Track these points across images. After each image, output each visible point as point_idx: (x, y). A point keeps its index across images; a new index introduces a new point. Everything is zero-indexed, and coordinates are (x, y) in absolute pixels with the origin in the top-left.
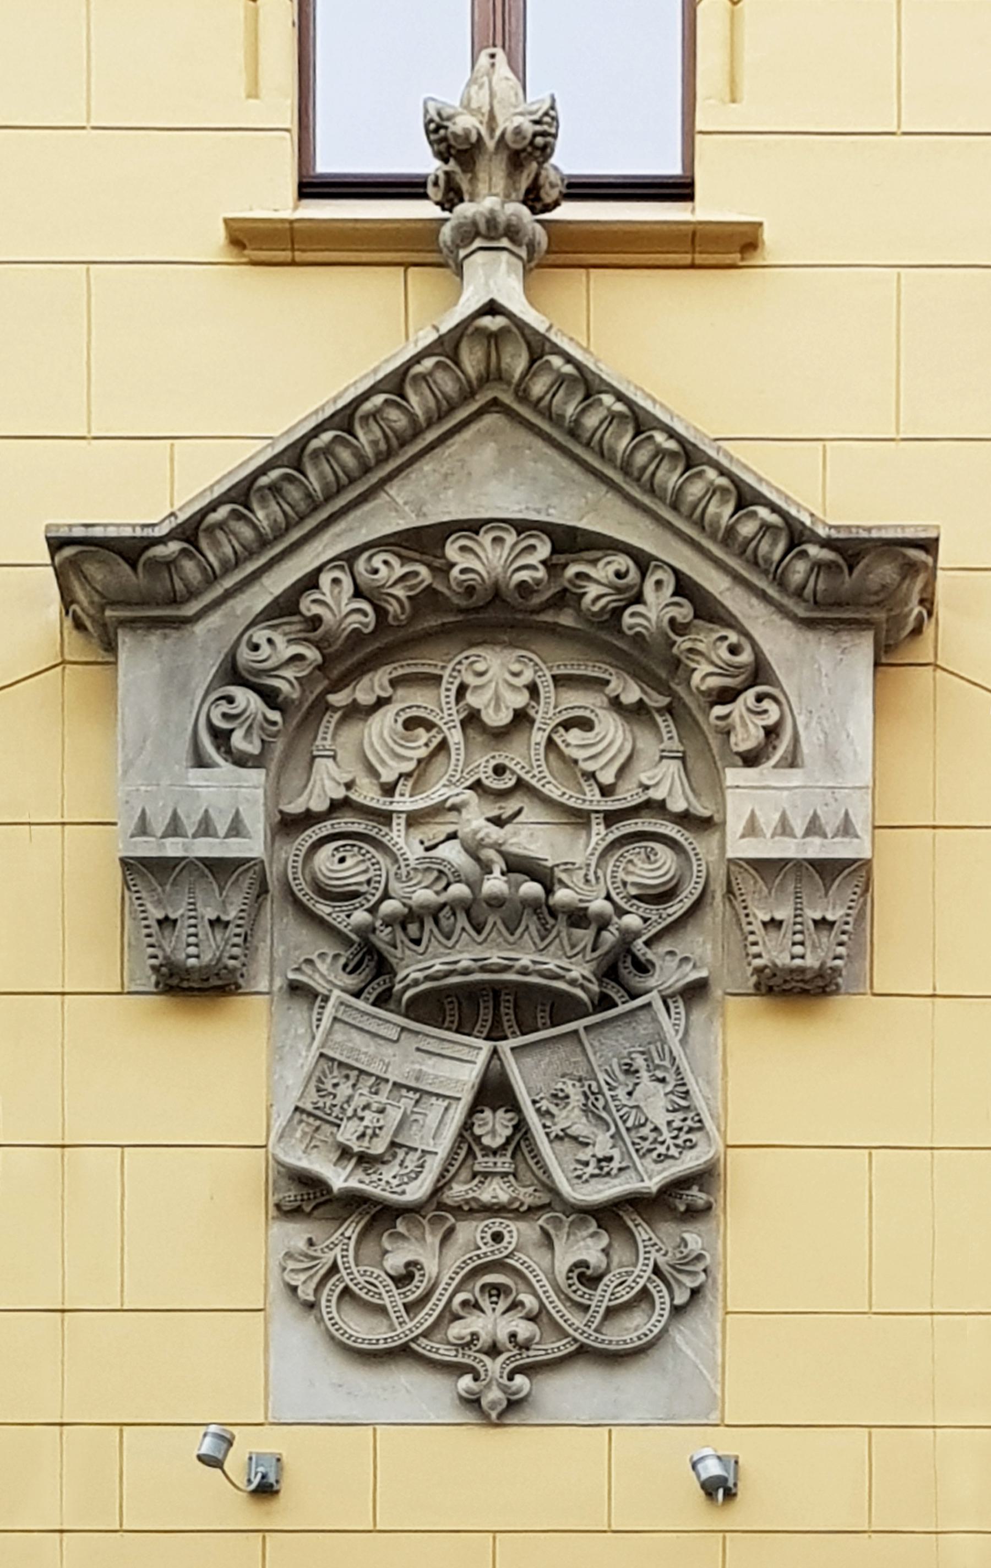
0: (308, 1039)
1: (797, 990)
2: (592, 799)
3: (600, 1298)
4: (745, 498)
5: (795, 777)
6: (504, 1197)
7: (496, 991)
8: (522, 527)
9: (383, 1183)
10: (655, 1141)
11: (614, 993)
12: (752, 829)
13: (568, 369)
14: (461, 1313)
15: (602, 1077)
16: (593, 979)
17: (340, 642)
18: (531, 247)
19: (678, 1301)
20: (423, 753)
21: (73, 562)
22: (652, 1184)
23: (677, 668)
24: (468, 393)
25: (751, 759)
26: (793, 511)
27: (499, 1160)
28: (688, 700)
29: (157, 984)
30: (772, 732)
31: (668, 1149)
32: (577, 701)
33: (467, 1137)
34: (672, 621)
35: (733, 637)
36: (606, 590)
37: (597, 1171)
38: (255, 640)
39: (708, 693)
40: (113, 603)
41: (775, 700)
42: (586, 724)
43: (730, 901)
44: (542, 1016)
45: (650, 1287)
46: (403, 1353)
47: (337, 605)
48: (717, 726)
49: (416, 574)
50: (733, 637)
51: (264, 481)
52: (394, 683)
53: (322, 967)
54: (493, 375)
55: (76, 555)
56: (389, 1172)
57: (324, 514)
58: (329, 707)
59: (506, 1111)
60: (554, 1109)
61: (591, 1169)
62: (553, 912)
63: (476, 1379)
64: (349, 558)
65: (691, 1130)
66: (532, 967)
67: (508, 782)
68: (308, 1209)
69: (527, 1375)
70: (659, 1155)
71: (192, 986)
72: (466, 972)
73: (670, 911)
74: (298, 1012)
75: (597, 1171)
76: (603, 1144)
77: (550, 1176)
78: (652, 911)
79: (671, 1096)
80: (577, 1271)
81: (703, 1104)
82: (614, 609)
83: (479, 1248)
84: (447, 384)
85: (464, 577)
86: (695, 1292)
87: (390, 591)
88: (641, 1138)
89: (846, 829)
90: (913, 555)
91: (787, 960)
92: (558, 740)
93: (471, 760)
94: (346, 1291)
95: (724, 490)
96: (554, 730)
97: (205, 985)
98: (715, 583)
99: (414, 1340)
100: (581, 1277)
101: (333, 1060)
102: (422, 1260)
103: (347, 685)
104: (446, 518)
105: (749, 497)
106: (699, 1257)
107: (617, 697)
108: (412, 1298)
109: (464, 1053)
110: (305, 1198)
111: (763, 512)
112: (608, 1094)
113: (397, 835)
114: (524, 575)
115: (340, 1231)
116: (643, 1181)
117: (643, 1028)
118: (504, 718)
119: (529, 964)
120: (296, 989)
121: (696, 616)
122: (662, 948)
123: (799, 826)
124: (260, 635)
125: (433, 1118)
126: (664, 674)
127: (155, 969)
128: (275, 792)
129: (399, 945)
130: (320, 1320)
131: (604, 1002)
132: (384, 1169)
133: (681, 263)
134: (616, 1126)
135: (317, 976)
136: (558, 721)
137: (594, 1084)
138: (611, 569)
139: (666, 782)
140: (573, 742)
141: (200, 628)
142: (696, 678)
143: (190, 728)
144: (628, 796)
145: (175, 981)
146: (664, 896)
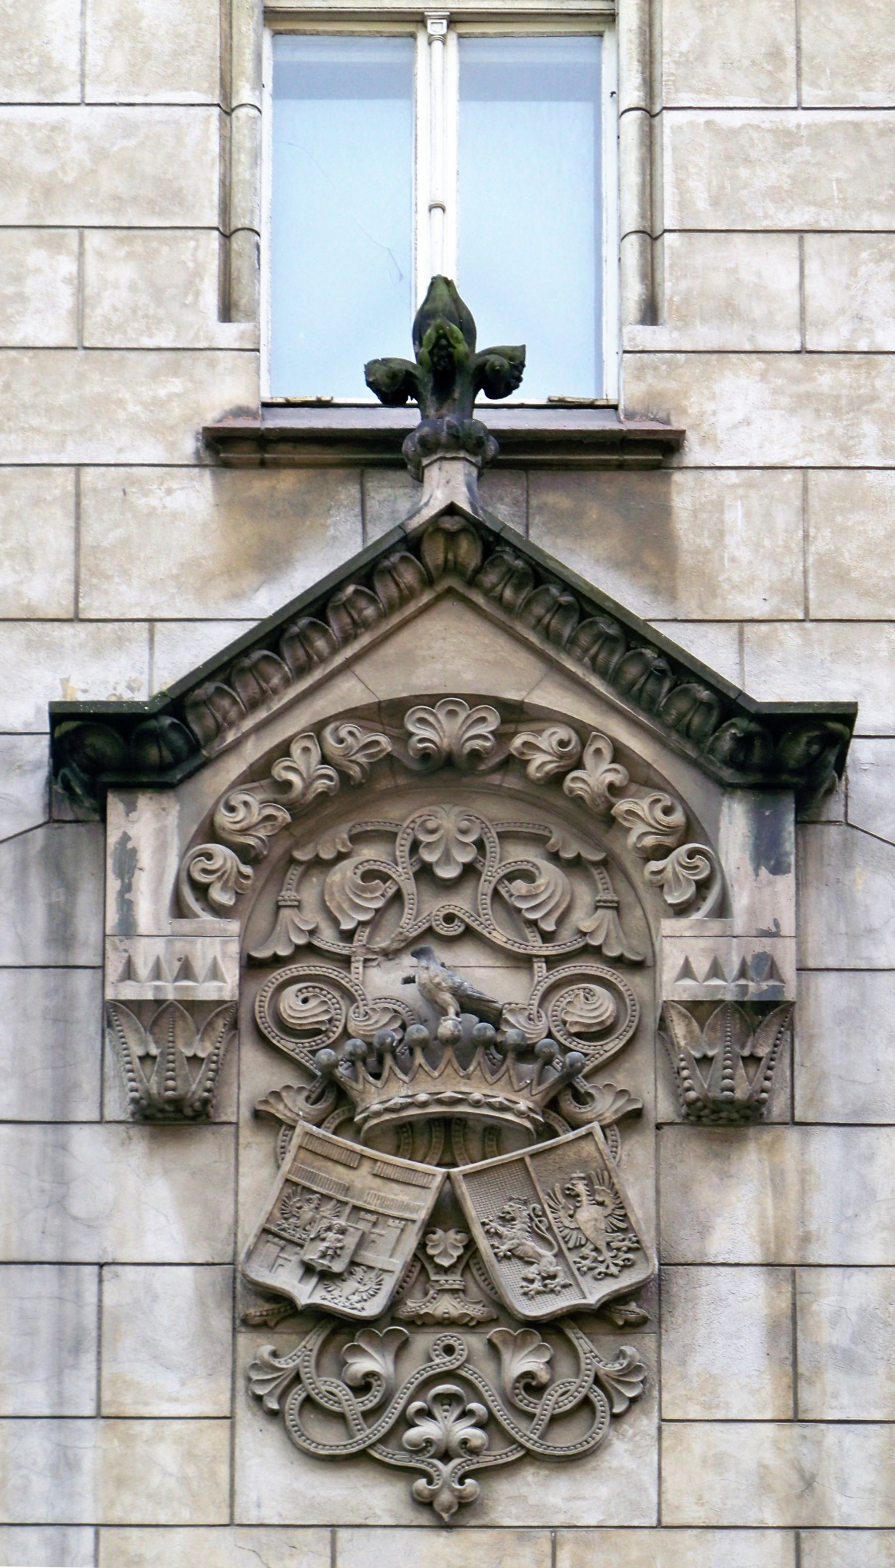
1: (726, 1119)
2: (536, 946)
8: (475, 700)
10: (595, 1260)
12: (687, 971)
19: (616, 1410)
25: (682, 910)
27: (450, 1278)
31: (608, 1267)
32: (522, 855)
33: (421, 1259)
35: (667, 801)
36: (549, 758)
38: (233, 803)
39: (643, 849)
41: (708, 859)
42: (528, 876)
44: (475, 1147)
45: (592, 1396)
47: (303, 771)
48: (651, 881)
49: (377, 743)
50: (667, 801)
58: (293, 861)
62: (500, 1047)
63: (430, 1482)
64: (318, 728)
65: (630, 1250)
66: (484, 1099)
67: (456, 929)
68: (272, 1324)
69: (477, 1479)
71: (170, 1118)
72: (424, 1104)
73: (606, 1048)
75: (541, 1288)
76: (548, 1259)
79: (610, 1219)
80: (523, 1382)
85: (421, 746)
86: (633, 1401)
87: (353, 758)
90: (831, 727)
92: (503, 891)
94: (309, 1401)
96: (500, 881)
99: (372, 1446)
107: (557, 852)
108: (370, 1406)
114: (477, 744)
115: (303, 1343)
116: (585, 1298)
119: (482, 1098)
122: (601, 1081)
124: (237, 799)
127: (134, 1101)
131: (548, 1132)
136: (502, 874)
138: (554, 740)
144: (567, 941)
146: (603, 1032)
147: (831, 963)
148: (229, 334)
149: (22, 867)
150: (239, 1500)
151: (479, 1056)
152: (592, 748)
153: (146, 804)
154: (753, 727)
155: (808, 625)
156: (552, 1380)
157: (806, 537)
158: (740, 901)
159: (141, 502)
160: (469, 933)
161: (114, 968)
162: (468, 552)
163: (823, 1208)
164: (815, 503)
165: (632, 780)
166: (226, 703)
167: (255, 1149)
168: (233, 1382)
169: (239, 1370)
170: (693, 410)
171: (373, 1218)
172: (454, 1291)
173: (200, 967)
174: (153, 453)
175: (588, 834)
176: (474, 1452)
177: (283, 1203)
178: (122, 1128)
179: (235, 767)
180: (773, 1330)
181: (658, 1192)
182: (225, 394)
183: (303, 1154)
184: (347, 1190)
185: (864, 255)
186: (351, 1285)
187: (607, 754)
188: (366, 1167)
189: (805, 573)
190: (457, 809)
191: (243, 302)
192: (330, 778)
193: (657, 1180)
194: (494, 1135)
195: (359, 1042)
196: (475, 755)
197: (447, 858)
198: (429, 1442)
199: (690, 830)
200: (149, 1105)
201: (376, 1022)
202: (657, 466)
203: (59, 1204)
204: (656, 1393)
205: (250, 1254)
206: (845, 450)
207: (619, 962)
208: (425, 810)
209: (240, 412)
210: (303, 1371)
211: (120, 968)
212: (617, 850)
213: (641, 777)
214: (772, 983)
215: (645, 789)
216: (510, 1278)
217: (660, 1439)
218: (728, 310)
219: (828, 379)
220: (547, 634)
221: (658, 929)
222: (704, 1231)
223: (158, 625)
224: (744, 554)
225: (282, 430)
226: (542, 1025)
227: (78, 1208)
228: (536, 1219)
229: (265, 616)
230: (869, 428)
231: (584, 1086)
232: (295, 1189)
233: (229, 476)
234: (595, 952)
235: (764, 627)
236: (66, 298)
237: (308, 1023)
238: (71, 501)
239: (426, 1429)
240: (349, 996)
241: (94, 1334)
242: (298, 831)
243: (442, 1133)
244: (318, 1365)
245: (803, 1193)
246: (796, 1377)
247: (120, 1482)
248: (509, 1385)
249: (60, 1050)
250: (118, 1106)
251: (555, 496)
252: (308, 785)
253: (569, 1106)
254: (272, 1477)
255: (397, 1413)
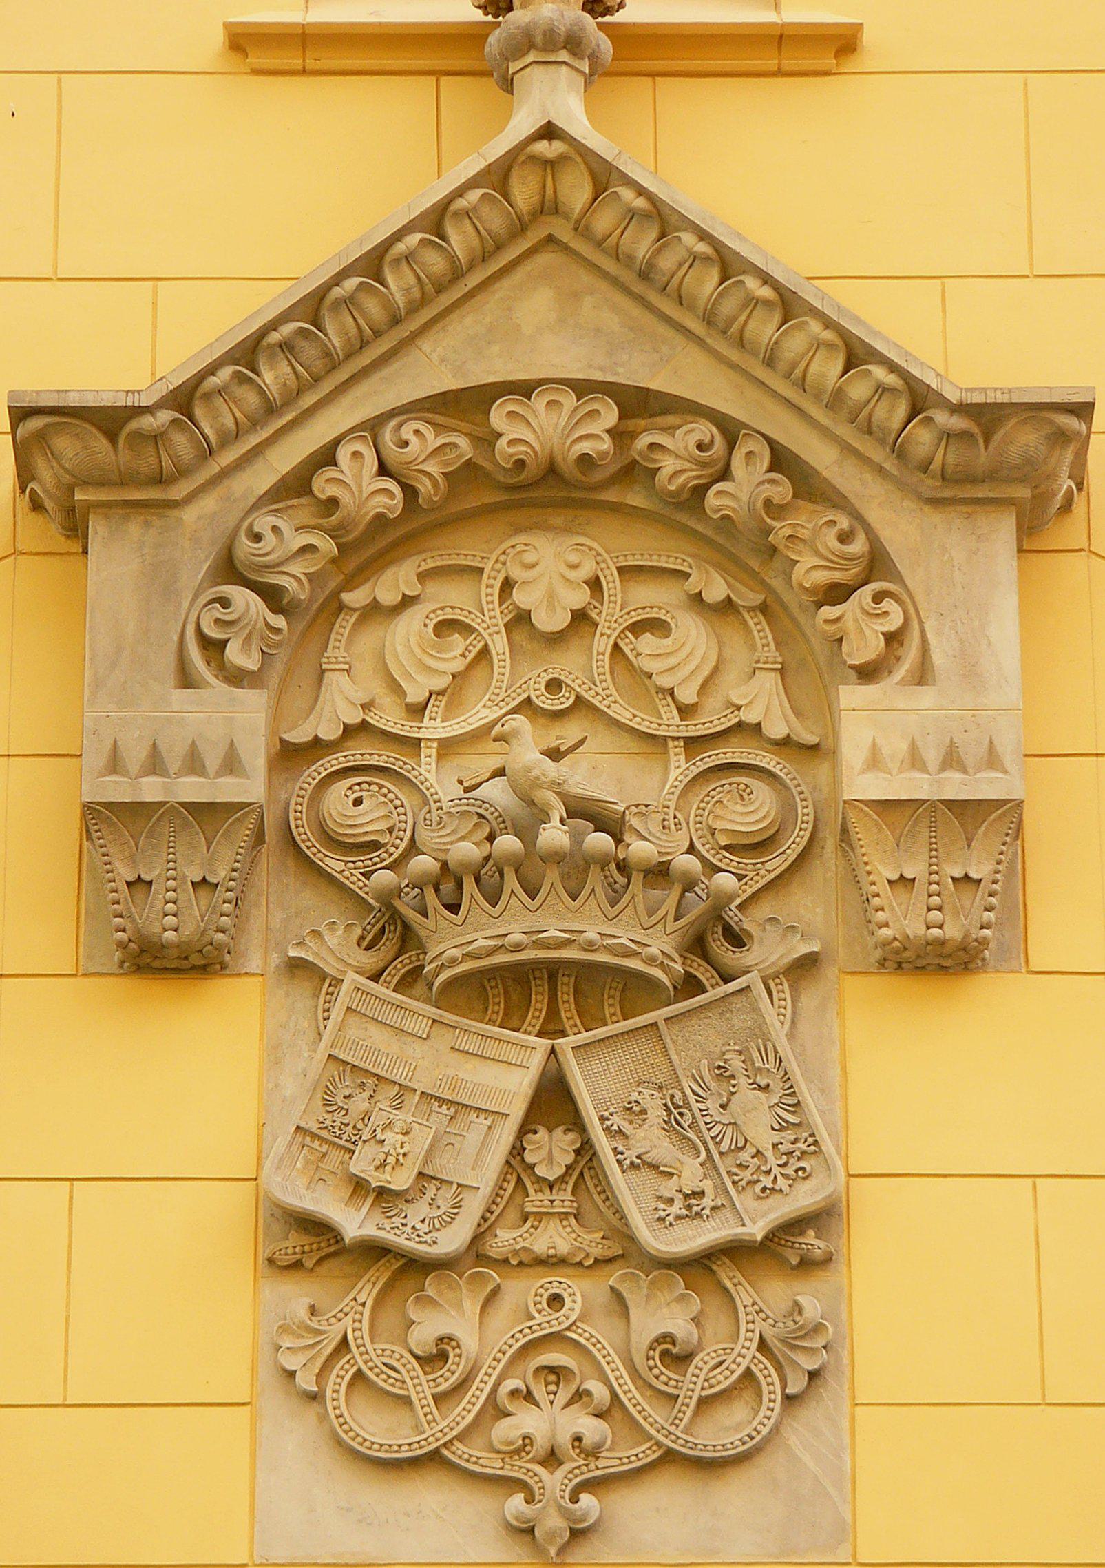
0: (312, 1035)
2: (669, 722)
3: (695, 1382)
4: (856, 355)
5: (926, 697)
6: (563, 1248)
7: (552, 971)
8: (582, 388)
9: (408, 1229)
11: (703, 973)
12: (874, 761)
13: (640, 203)
14: (510, 1408)
15: (687, 1084)
16: (676, 956)
17: (361, 527)
18: (594, 58)
20: (459, 665)
21: (41, 437)
22: (756, 1231)
23: (772, 557)
24: (520, 227)
25: (867, 673)
26: (916, 372)
28: (787, 597)
29: (122, 963)
32: (651, 597)
34: (768, 503)
35: (844, 523)
36: (687, 465)
37: (684, 1212)
38: (256, 529)
40: (85, 483)
41: (898, 600)
43: (844, 851)
46: (434, 1459)
47: (359, 486)
48: (825, 632)
49: (455, 445)
50: (844, 523)
51: (274, 337)
52: (423, 577)
53: (332, 940)
54: (549, 207)
55: (46, 426)
56: (418, 1212)
57: (342, 375)
59: (565, 1132)
60: (627, 1129)
61: (677, 1208)
62: (623, 867)
63: (529, 1500)
64: (372, 427)
67: (564, 701)
70: (764, 1189)
71: (165, 962)
72: (518, 948)
73: (769, 866)
74: (300, 997)
75: (684, 1212)
76: (691, 1174)
77: (623, 1217)
78: (746, 862)
81: (819, 1120)
82: (695, 488)
83: (533, 1318)
84: (495, 220)
86: (813, 1375)
88: (740, 1165)
89: (992, 760)
91: (921, 930)
93: (516, 675)
94: (359, 1374)
95: (830, 346)
97: (185, 964)
98: (820, 456)
100: (665, 1354)
101: (346, 1063)
102: (459, 1333)
103: (369, 579)
104: (491, 379)
105: (860, 352)
106: (818, 1328)
108: (444, 1387)
109: (512, 1054)
110: (306, 1245)
111: (879, 373)
112: (695, 1106)
113: (427, 770)
114: (586, 447)
115: (351, 1296)
116: (744, 1225)
117: (741, 1020)
118: (561, 620)
120: (296, 967)
121: (795, 496)
122: (763, 910)
123: (933, 757)
124: (263, 522)
125: (474, 1137)
126: (755, 564)
128: (276, 714)
129: (431, 913)
130: (324, 1417)
131: (690, 986)
132: (409, 1209)
133: (765, 68)
134: (707, 1150)
135: (324, 953)
137: (678, 1095)
138: (693, 439)
139: (764, 701)
140: (646, 650)
141: (189, 515)
142: (799, 572)
143: (176, 638)
144: (711, 720)
145: (147, 959)
146: (760, 846)
152: (744, 450)
176: (593, 1453)
192: (391, 495)
194: (633, 989)
201: (453, 832)
216: (634, 1198)
228: (675, 1112)
239: (528, 1422)
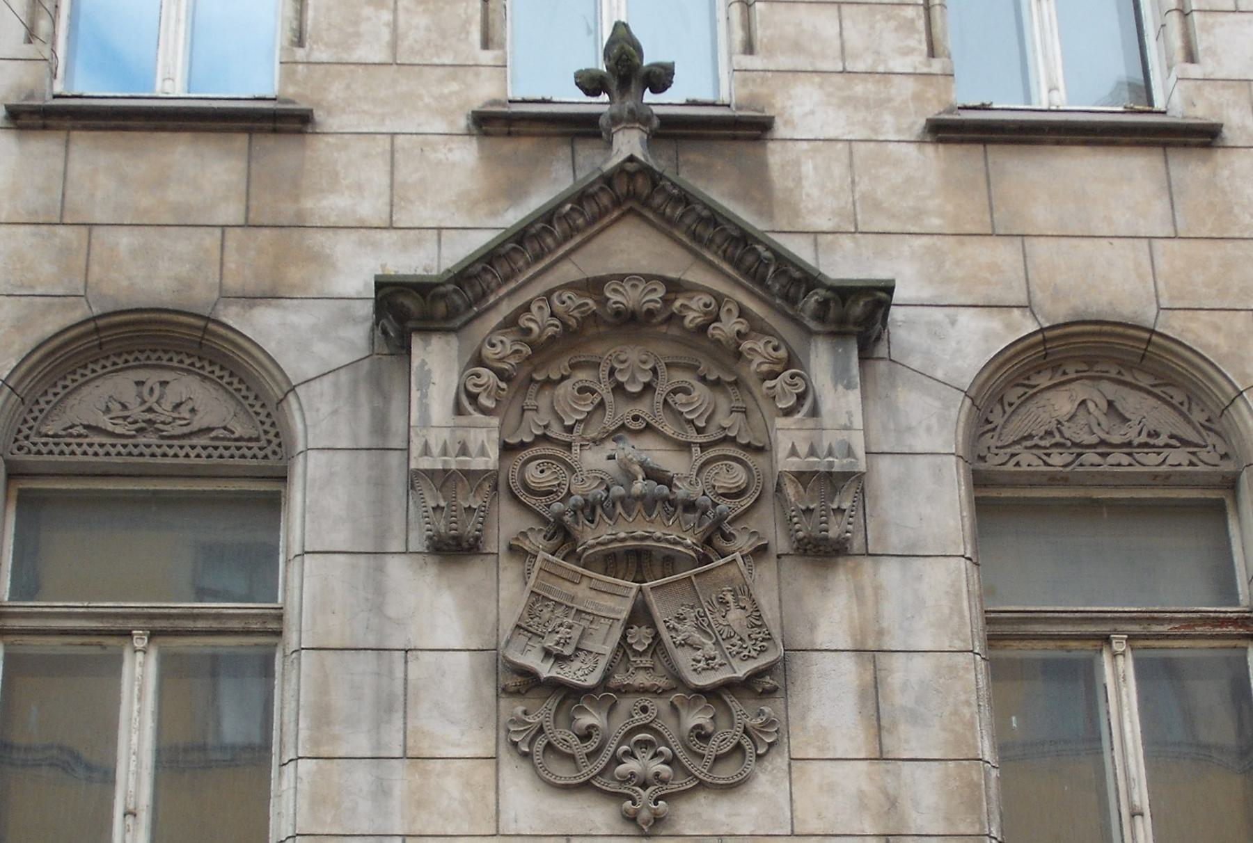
1: (822, 552)
3: (712, 748)
8: (649, 278)
12: (793, 452)
19: (760, 752)
20: (589, 409)
25: (788, 412)
30: (801, 397)
33: (624, 646)
36: (696, 314)
39: (761, 373)
42: (686, 391)
44: (657, 571)
46: (586, 787)
47: (539, 322)
50: (776, 342)
58: (532, 380)
61: (702, 664)
62: (673, 503)
63: (634, 804)
64: (548, 294)
65: (764, 640)
71: (452, 549)
72: (623, 540)
86: (771, 745)
90: (878, 297)
94: (549, 746)
96: (668, 394)
99: (594, 777)
114: (651, 305)
122: (740, 526)
127: (430, 538)
144: (713, 434)
146: (739, 494)
147: (886, 449)
148: (487, 57)
149: (355, 383)
150: (503, 817)
151: (659, 507)
153: (437, 342)
154: (829, 294)
155: (858, 235)
156: (715, 731)
157: (853, 182)
158: (826, 406)
159: (432, 156)
160: (649, 427)
161: (416, 447)
162: (642, 185)
163: (891, 612)
164: (857, 161)
165: (752, 329)
166: (489, 277)
167: (510, 573)
168: (497, 734)
169: (501, 724)
170: (778, 105)
171: (591, 618)
172: (646, 669)
173: (473, 448)
174: (440, 126)
175: (722, 363)
176: (664, 782)
177: (530, 607)
178: (420, 556)
179: (495, 319)
180: (862, 695)
181: (780, 600)
182: (484, 92)
183: (542, 573)
184: (573, 599)
185: (878, 17)
186: (577, 664)
187: (735, 312)
188: (585, 583)
189: (854, 204)
190: (639, 348)
191: (496, 39)
193: (780, 593)
194: (670, 562)
195: (579, 497)
196: (651, 313)
197: (633, 379)
198: (632, 774)
199: (790, 362)
200: (439, 541)
202: (756, 139)
203: (378, 608)
204: (786, 740)
205: (508, 642)
206: (874, 130)
207: (748, 447)
208: (618, 348)
209: (495, 102)
210: (545, 724)
211: (420, 447)
212: (744, 374)
213: (757, 328)
214: (850, 460)
215: (760, 335)
216: (684, 659)
217: (790, 772)
218: (797, 47)
219: (859, 88)
220: (695, 237)
221: (772, 426)
222: (813, 627)
223: (444, 232)
224: (815, 192)
225: (522, 113)
226: (699, 488)
227: (392, 611)
229: (509, 226)
230: (888, 118)
231: (729, 529)
232: (537, 597)
233: (488, 141)
234: (732, 441)
235: (830, 237)
236: (386, 35)
237: (545, 486)
238: (388, 157)
239: (631, 766)
240: (572, 470)
241: (402, 699)
242: (536, 361)
243: (635, 561)
244: (555, 721)
245: (877, 602)
246: (880, 728)
247: (420, 804)
248: (686, 734)
249: (379, 504)
250: (418, 542)
251: (694, 155)
252: (542, 331)
253: (720, 543)
254: (525, 801)
255: (610, 754)
